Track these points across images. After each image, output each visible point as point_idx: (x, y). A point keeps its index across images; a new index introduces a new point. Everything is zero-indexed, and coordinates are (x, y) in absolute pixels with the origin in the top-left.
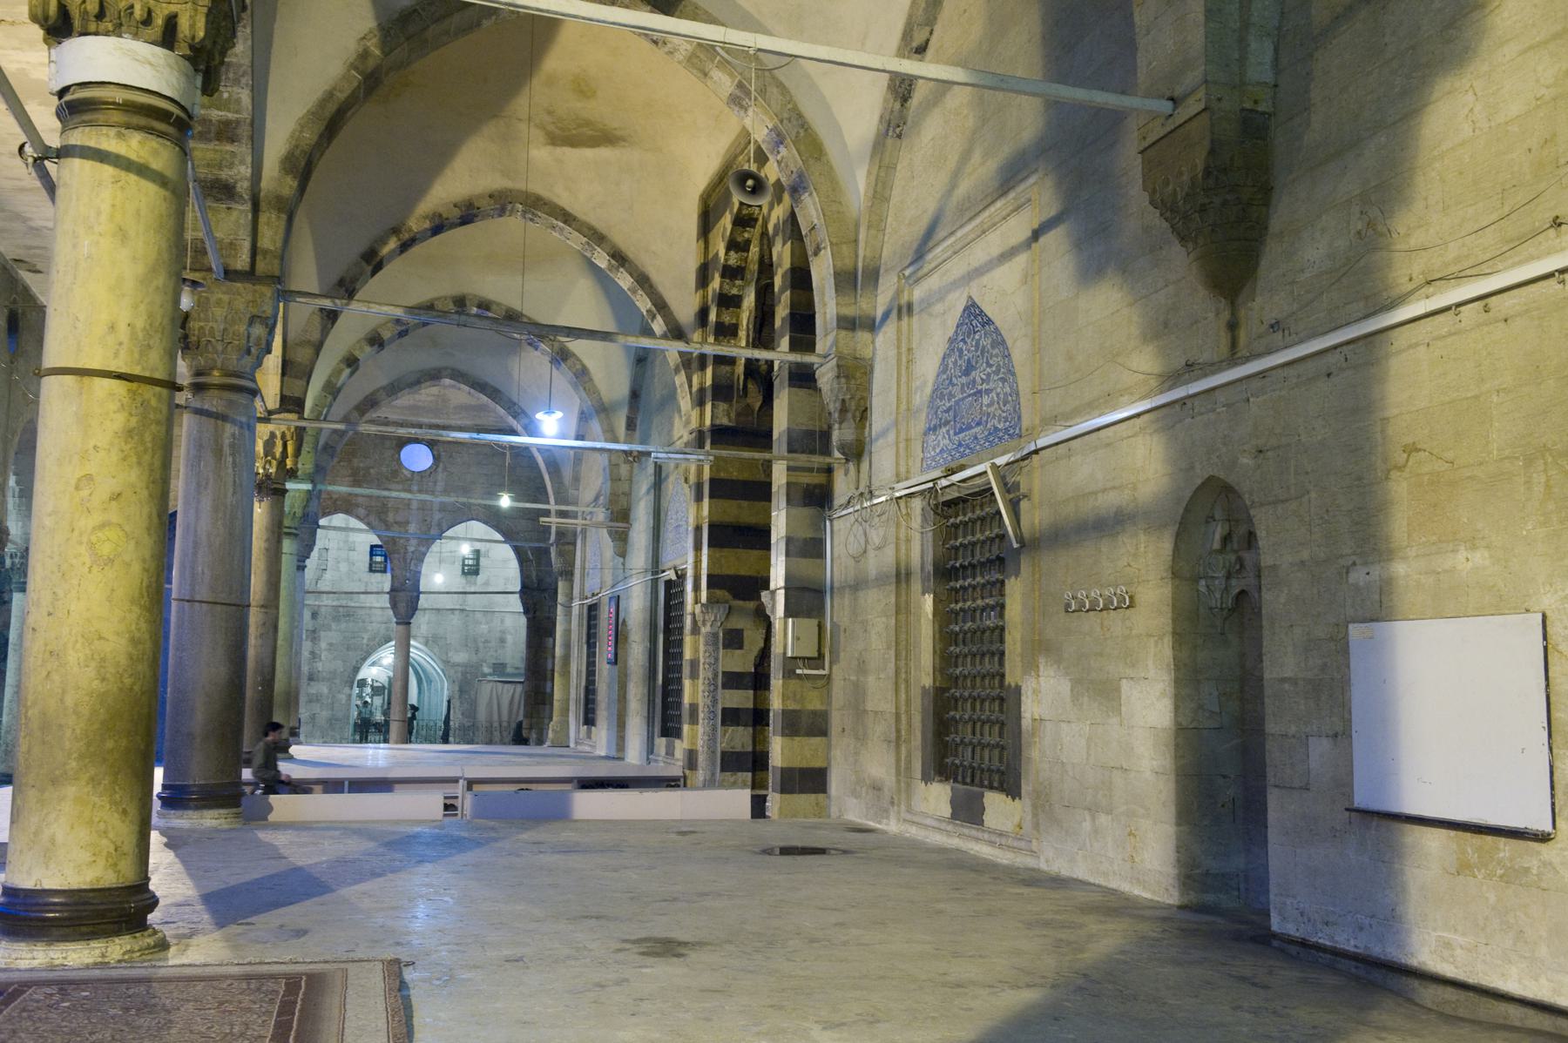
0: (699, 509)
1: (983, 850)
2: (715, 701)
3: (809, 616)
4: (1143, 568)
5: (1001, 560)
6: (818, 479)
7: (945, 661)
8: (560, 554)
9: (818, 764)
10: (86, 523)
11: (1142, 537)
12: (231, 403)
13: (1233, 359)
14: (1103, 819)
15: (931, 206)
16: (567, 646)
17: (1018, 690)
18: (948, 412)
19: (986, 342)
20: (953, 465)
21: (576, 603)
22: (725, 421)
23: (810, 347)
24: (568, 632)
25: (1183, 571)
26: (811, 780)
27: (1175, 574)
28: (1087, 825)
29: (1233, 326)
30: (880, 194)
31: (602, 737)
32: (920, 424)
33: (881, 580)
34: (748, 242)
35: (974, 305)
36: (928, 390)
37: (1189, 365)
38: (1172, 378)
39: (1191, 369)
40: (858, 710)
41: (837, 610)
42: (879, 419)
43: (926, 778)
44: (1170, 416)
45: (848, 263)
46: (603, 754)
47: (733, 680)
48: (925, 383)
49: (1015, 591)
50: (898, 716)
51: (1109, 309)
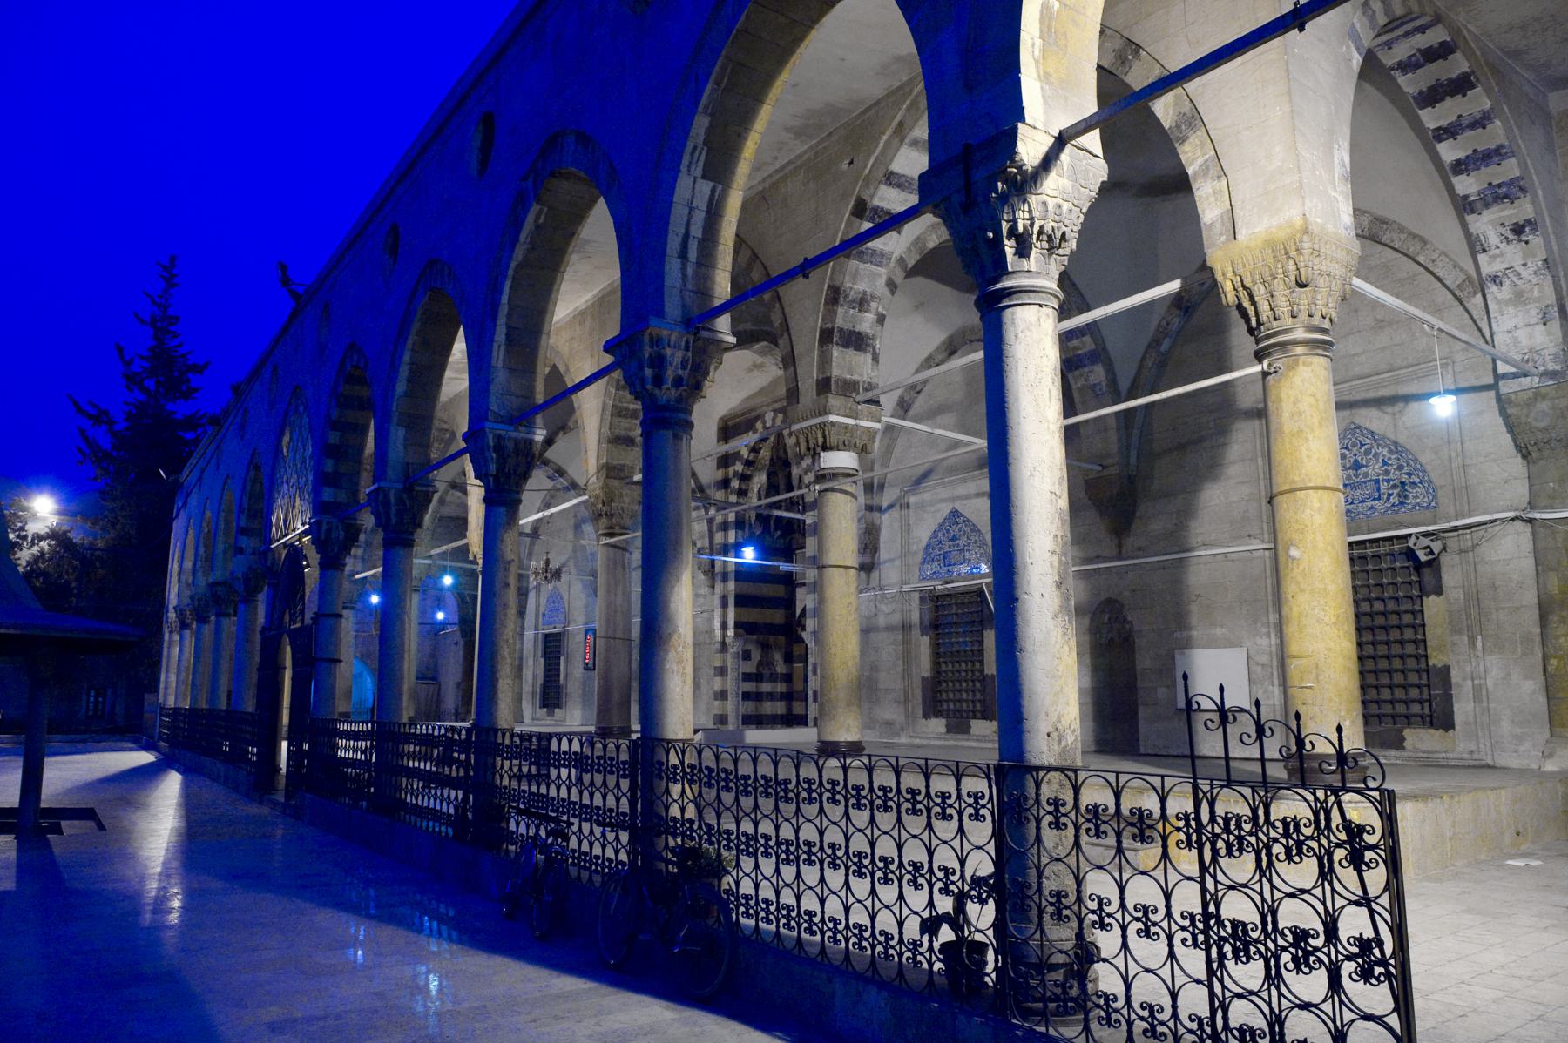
7: (936, 664)
13: (1120, 558)
21: (529, 634)
29: (1120, 546)
36: (924, 544)
39: (1098, 558)
42: (884, 554)
43: (926, 716)
47: (747, 677)
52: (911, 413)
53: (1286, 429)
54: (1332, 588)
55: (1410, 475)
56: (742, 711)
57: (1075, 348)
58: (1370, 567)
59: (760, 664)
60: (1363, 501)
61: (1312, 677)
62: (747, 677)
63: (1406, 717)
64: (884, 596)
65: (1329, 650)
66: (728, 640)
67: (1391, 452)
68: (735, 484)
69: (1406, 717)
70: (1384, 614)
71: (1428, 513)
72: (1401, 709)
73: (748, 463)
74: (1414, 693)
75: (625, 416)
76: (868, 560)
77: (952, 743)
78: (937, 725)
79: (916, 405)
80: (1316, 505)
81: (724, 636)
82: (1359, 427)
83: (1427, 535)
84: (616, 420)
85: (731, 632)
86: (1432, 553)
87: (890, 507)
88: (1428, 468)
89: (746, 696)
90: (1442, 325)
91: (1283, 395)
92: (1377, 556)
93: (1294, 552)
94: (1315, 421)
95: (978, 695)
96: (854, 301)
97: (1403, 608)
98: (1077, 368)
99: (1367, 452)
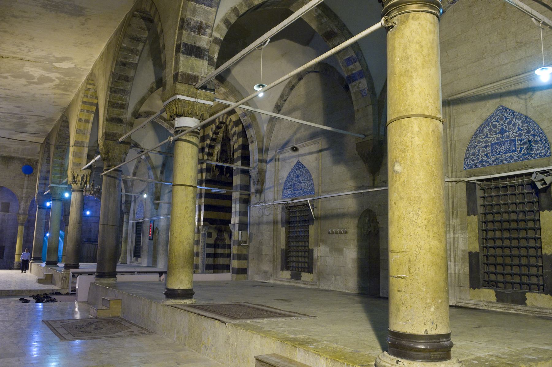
0: (200, 200)
1: (302, 285)
2: (204, 251)
3: (244, 230)
4: (351, 227)
5: (309, 220)
6: (246, 197)
7: (288, 242)
8: (126, 207)
9: (245, 267)
10: (187, 216)
11: (350, 219)
12: (118, 174)
13: (374, 187)
14: (338, 277)
15: (287, 138)
16: (127, 234)
17: (312, 250)
18: (290, 185)
19: (304, 172)
20: (294, 198)
21: (131, 222)
22: (209, 178)
23: (248, 165)
24: (127, 230)
25: (360, 227)
26: (243, 271)
27: (358, 227)
28: (333, 278)
29: (374, 180)
30: (271, 131)
31: (144, 261)
32: (282, 187)
33: (268, 223)
34: (219, 132)
35: (300, 162)
36: (284, 180)
37: (363, 186)
38: (358, 188)
39: (363, 187)
40: (259, 253)
41: (252, 229)
42: (267, 185)
43: (282, 269)
44: (357, 196)
45: (261, 146)
46: (145, 265)
47: (209, 246)
48: (283, 178)
49: (312, 230)
50: (273, 256)
51: (340, 171)
52: (282, 111)
53: (397, 70)
54: (425, 196)
55: (534, 136)
56: (206, 263)
57: (352, 70)
58: (509, 192)
59: (216, 240)
60: (506, 153)
61: (406, 269)
62: (209, 246)
63: (528, 285)
64: (266, 206)
65: (420, 247)
66: (200, 227)
67: (523, 122)
68: (207, 150)
69: (528, 285)
70: (516, 221)
71: (545, 160)
72: (525, 279)
73: (213, 140)
74: (533, 271)
75: (116, 107)
76: (259, 187)
77: (292, 284)
78: (287, 274)
79: (284, 108)
80: (416, 129)
81: (199, 224)
82: (505, 108)
83: (543, 172)
84: (111, 109)
85: (202, 223)
86: (545, 183)
87: (271, 160)
88: (546, 131)
89: (208, 255)
90: (546, 20)
91: (397, 45)
92: (512, 186)
93: (397, 168)
94: (419, 62)
95: (307, 260)
96: (194, 27)
97: (528, 218)
98: (353, 81)
99: (509, 123)
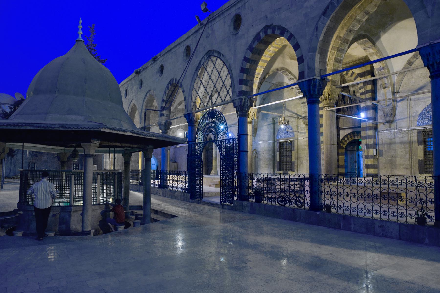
7: (425, 155)
36: (419, 113)
79: (415, 63)
